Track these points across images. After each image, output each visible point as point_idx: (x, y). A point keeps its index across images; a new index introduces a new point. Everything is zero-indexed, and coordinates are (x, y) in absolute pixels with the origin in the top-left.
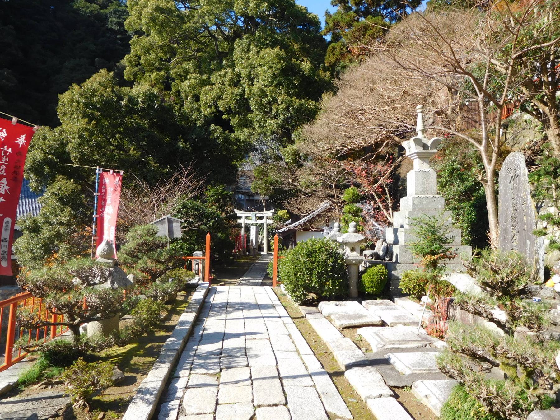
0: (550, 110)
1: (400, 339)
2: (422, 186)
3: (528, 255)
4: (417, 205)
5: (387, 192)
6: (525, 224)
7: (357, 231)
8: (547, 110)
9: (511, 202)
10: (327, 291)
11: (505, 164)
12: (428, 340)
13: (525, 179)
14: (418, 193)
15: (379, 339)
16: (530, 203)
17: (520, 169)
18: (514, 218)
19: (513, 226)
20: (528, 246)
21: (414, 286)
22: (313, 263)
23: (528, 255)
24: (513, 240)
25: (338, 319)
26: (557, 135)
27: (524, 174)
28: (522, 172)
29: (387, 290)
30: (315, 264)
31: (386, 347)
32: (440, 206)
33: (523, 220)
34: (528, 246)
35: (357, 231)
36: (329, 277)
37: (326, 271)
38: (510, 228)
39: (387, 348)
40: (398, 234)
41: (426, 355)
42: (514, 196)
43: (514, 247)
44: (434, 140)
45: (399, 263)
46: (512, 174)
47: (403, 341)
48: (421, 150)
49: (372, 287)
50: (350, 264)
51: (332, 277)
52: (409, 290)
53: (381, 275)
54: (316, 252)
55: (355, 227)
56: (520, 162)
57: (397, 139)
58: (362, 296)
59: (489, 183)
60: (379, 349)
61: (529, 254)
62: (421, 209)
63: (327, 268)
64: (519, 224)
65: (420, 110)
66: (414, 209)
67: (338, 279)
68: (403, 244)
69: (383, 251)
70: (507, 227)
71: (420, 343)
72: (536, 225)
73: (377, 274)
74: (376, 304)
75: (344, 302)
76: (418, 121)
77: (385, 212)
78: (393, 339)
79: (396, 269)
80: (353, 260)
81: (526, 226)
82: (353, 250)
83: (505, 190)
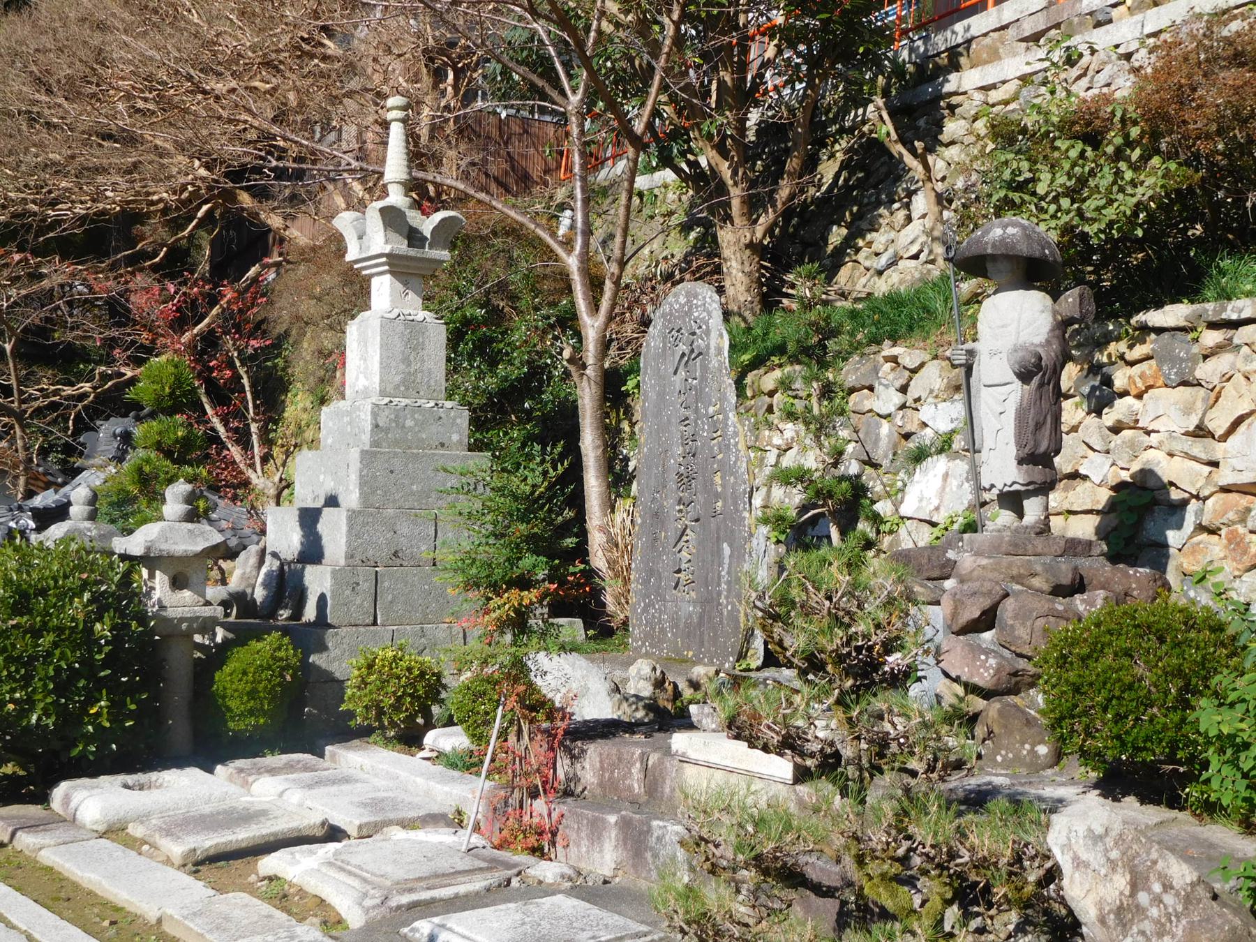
0: (735, 173)
1: (424, 870)
2: (402, 367)
3: (724, 586)
4: (387, 430)
5: (245, 381)
6: (717, 496)
7: (192, 516)
8: (725, 169)
9: (676, 430)
10: (89, 739)
11: (663, 316)
12: (508, 866)
13: (721, 363)
14: (389, 389)
15: (356, 883)
16: (736, 434)
17: (708, 332)
18: (685, 479)
19: (680, 502)
20: (727, 561)
21: (399, 699)
22: (36, 633)
23: (724, 586)
24: (682, 543)
25: (168, 832)
26: (748, 246)
27: (719, 350)
28: (713, 344)
29: (304, 717)
30: (47, 640)
31: (393, 903)
32: (455, 437)
33: (712, 483)
34: (727, 561)
35: (192, 516)
36: (101, 683)
37: (89, 667)
38: (670, 505)
39: (399, 907)
40: (320, 527)
41: (532, 908)
42: (687, 413)
43: (684, 566)
44: (443, 220)
45: (330, 626)
46: (683, 348)
47: (436, 876)
48: (402, 246)
49: (251, 712)
50: (175, 632)
51: (111, 685)
52: (380, 713)
53: (283, 669)
54: (43, 592)
55: (190, 499)
56: (709, 314)
57: (245, 199)
58: (210, 747)
59: (589, 371)
60: (372, 914)
61: (729, 583)
62: (397, 443)
63: (90, 651)
64: (700, 498)
65: (400, 114)
66: (375, 443)
67: (131, 689)
68: (342, 562)
69: (265, 585)
70: (662, 506)
71: (489, 875)
72: (750, 497)
73: (269, 668)
74: (272, 771)
75: (154, 776)
76: (390, 140)
77: (235, 452)
78: (401, 874)
79: (322, 648)
80: (182, 620)
81: (719, 504)
82: (177, 583)
83: (661, 395)
